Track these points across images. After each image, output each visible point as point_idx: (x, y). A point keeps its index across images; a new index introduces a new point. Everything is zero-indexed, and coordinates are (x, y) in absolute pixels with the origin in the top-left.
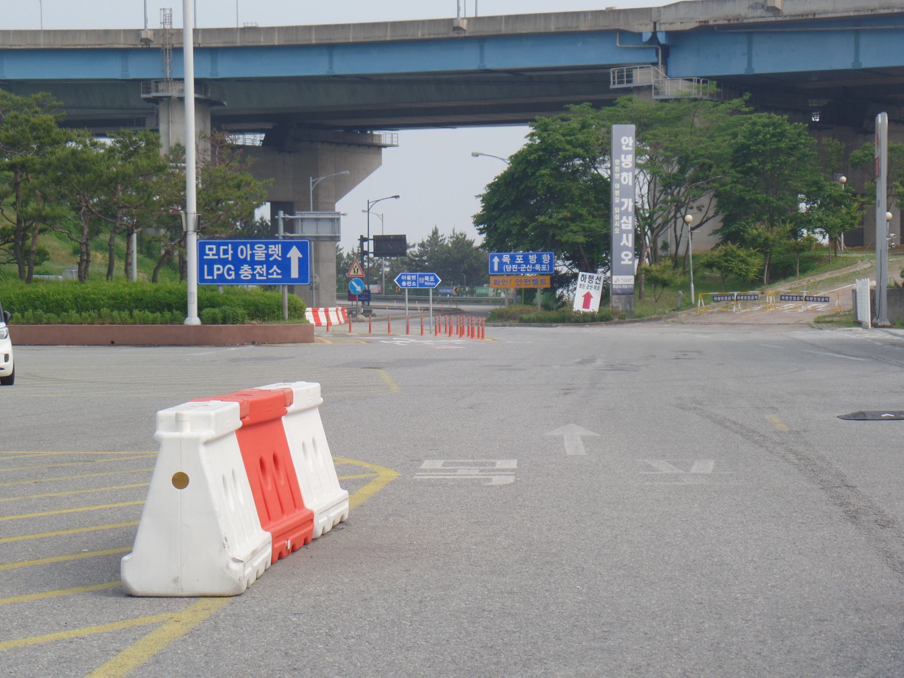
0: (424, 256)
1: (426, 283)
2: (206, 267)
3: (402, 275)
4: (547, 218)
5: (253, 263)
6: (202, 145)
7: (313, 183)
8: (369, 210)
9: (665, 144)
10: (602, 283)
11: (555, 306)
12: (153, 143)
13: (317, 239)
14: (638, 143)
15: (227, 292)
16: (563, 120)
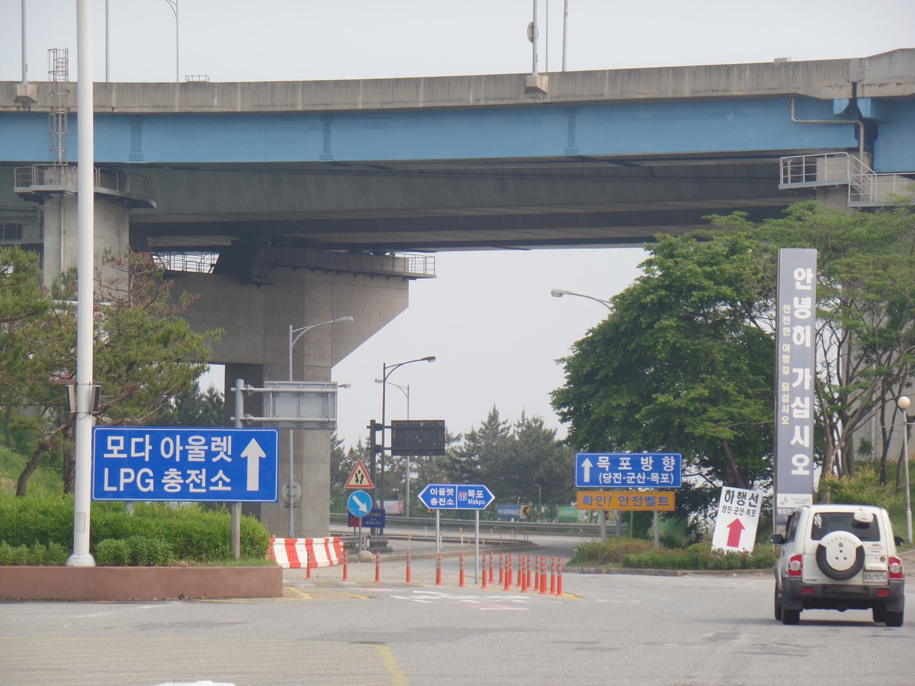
0: (474, 455)
1: (470, 502)
2: (106, 470)
3: (430, 487)
4: (672, 398)
5: (184, 466)
6: (109, 272)
7: (295, 335)
8: (385, 379)
9: (866, 281)
10: (759, 505)
11: (684, 541)
12: (25, 269)
13: (299, 425)
14: (822, 278)
15: (140, 513)
16: (700, 239)
